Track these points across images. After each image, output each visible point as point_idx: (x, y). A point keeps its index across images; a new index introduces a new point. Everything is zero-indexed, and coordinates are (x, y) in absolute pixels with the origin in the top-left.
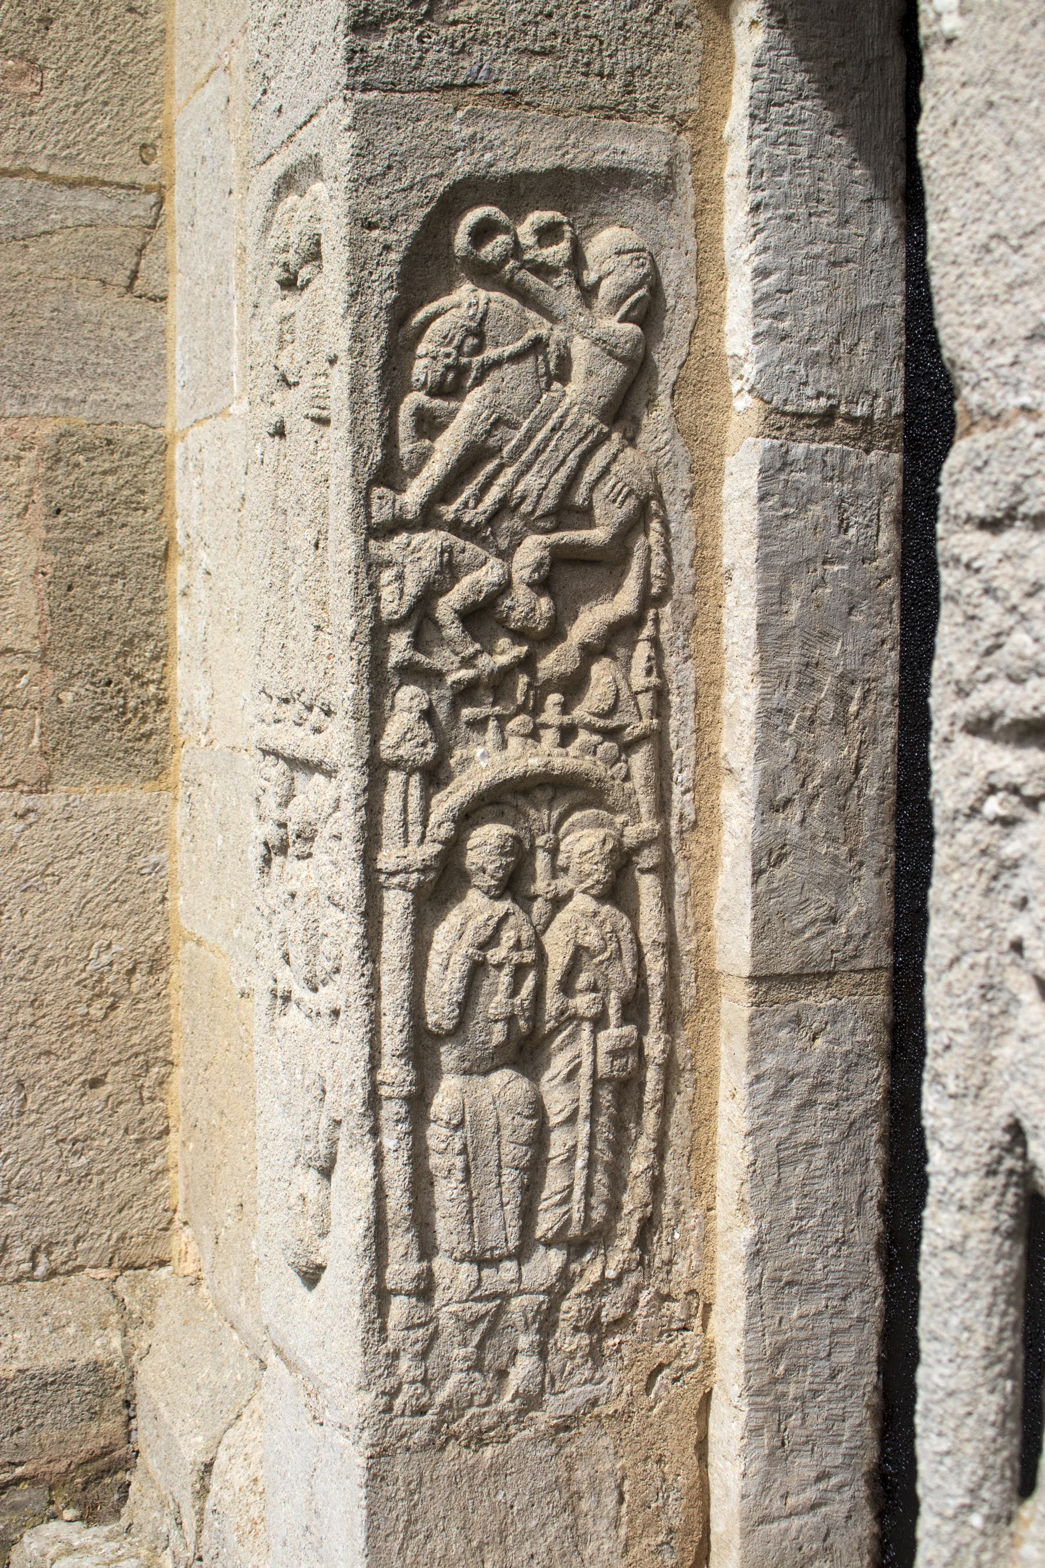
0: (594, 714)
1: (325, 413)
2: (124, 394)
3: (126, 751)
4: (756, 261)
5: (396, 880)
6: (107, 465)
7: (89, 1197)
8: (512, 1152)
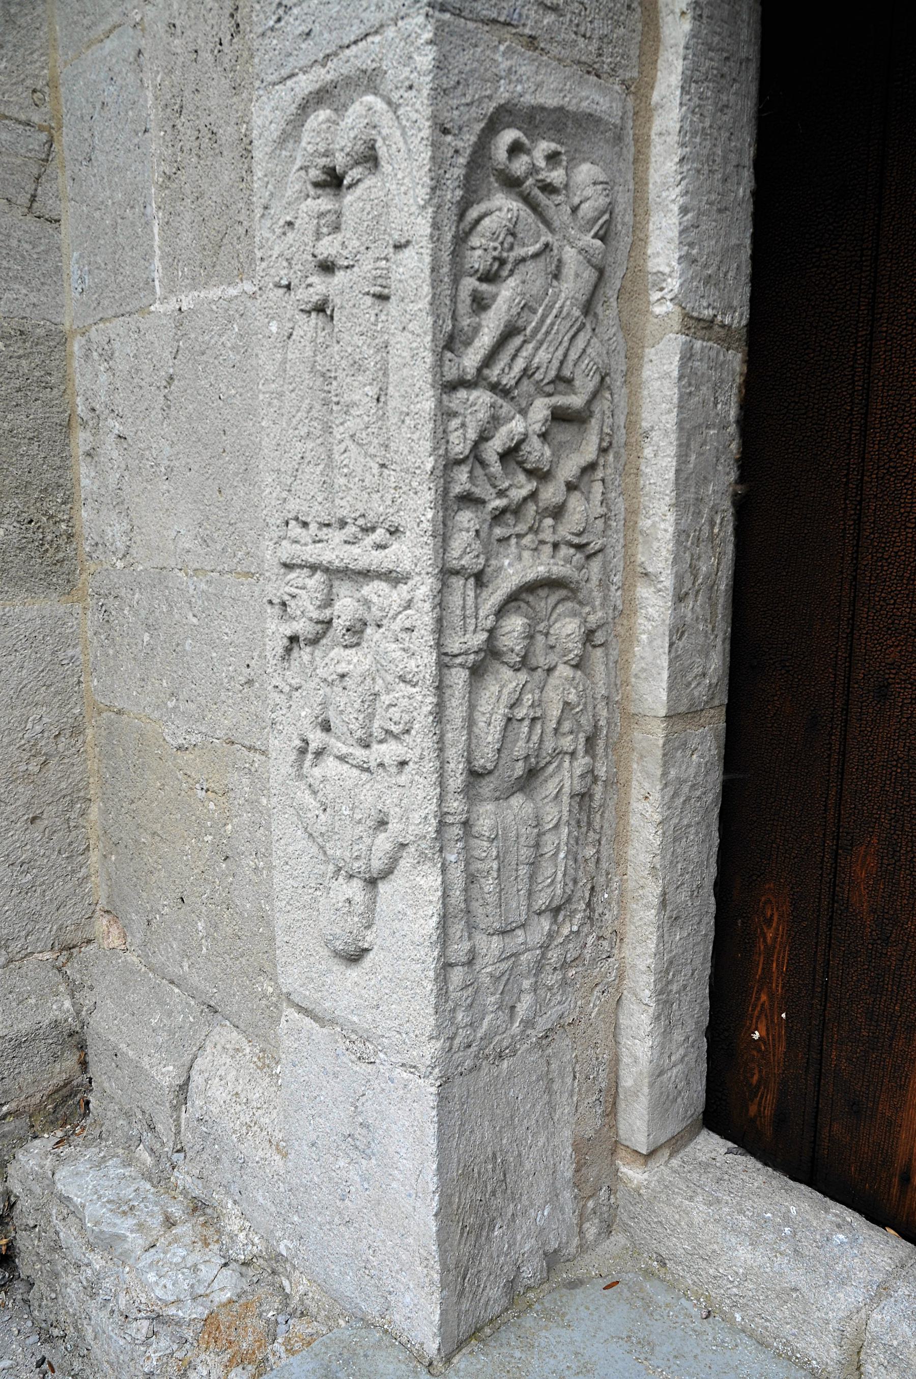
0: (573, 534)
1: (386, 291)
2: (31, 296)
3: (46, 574)
4: (681, 201)
5: (459, 660)
6: (21, 352)
7: (34, 902)
8: (525, 853)
